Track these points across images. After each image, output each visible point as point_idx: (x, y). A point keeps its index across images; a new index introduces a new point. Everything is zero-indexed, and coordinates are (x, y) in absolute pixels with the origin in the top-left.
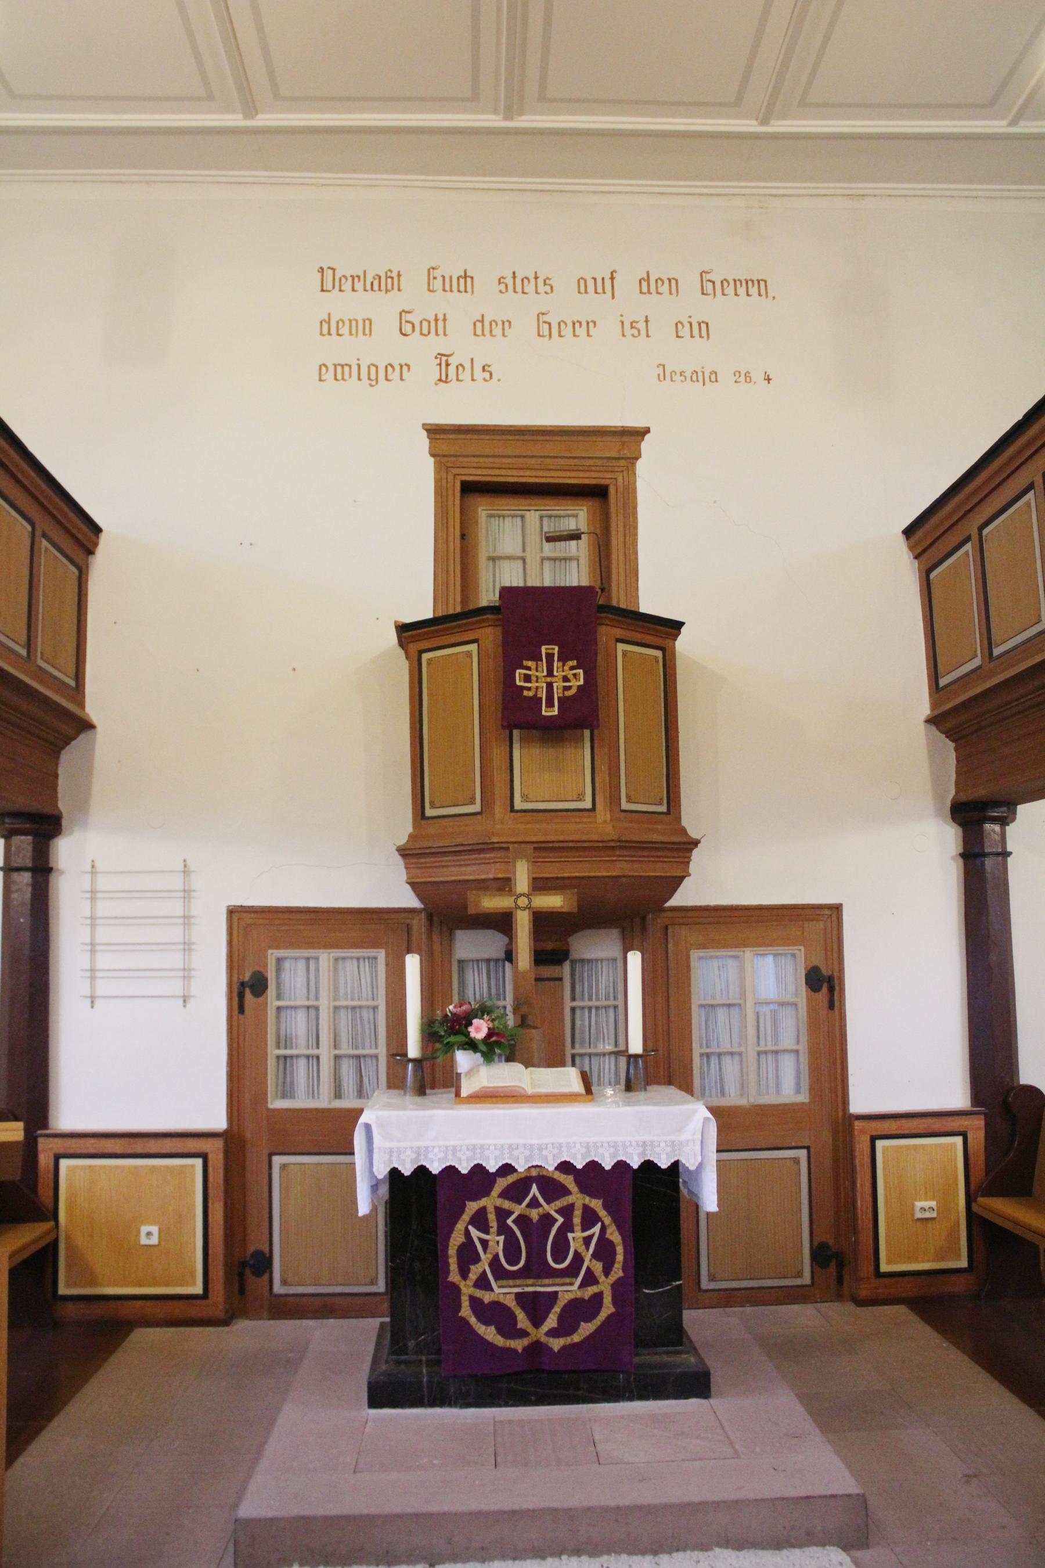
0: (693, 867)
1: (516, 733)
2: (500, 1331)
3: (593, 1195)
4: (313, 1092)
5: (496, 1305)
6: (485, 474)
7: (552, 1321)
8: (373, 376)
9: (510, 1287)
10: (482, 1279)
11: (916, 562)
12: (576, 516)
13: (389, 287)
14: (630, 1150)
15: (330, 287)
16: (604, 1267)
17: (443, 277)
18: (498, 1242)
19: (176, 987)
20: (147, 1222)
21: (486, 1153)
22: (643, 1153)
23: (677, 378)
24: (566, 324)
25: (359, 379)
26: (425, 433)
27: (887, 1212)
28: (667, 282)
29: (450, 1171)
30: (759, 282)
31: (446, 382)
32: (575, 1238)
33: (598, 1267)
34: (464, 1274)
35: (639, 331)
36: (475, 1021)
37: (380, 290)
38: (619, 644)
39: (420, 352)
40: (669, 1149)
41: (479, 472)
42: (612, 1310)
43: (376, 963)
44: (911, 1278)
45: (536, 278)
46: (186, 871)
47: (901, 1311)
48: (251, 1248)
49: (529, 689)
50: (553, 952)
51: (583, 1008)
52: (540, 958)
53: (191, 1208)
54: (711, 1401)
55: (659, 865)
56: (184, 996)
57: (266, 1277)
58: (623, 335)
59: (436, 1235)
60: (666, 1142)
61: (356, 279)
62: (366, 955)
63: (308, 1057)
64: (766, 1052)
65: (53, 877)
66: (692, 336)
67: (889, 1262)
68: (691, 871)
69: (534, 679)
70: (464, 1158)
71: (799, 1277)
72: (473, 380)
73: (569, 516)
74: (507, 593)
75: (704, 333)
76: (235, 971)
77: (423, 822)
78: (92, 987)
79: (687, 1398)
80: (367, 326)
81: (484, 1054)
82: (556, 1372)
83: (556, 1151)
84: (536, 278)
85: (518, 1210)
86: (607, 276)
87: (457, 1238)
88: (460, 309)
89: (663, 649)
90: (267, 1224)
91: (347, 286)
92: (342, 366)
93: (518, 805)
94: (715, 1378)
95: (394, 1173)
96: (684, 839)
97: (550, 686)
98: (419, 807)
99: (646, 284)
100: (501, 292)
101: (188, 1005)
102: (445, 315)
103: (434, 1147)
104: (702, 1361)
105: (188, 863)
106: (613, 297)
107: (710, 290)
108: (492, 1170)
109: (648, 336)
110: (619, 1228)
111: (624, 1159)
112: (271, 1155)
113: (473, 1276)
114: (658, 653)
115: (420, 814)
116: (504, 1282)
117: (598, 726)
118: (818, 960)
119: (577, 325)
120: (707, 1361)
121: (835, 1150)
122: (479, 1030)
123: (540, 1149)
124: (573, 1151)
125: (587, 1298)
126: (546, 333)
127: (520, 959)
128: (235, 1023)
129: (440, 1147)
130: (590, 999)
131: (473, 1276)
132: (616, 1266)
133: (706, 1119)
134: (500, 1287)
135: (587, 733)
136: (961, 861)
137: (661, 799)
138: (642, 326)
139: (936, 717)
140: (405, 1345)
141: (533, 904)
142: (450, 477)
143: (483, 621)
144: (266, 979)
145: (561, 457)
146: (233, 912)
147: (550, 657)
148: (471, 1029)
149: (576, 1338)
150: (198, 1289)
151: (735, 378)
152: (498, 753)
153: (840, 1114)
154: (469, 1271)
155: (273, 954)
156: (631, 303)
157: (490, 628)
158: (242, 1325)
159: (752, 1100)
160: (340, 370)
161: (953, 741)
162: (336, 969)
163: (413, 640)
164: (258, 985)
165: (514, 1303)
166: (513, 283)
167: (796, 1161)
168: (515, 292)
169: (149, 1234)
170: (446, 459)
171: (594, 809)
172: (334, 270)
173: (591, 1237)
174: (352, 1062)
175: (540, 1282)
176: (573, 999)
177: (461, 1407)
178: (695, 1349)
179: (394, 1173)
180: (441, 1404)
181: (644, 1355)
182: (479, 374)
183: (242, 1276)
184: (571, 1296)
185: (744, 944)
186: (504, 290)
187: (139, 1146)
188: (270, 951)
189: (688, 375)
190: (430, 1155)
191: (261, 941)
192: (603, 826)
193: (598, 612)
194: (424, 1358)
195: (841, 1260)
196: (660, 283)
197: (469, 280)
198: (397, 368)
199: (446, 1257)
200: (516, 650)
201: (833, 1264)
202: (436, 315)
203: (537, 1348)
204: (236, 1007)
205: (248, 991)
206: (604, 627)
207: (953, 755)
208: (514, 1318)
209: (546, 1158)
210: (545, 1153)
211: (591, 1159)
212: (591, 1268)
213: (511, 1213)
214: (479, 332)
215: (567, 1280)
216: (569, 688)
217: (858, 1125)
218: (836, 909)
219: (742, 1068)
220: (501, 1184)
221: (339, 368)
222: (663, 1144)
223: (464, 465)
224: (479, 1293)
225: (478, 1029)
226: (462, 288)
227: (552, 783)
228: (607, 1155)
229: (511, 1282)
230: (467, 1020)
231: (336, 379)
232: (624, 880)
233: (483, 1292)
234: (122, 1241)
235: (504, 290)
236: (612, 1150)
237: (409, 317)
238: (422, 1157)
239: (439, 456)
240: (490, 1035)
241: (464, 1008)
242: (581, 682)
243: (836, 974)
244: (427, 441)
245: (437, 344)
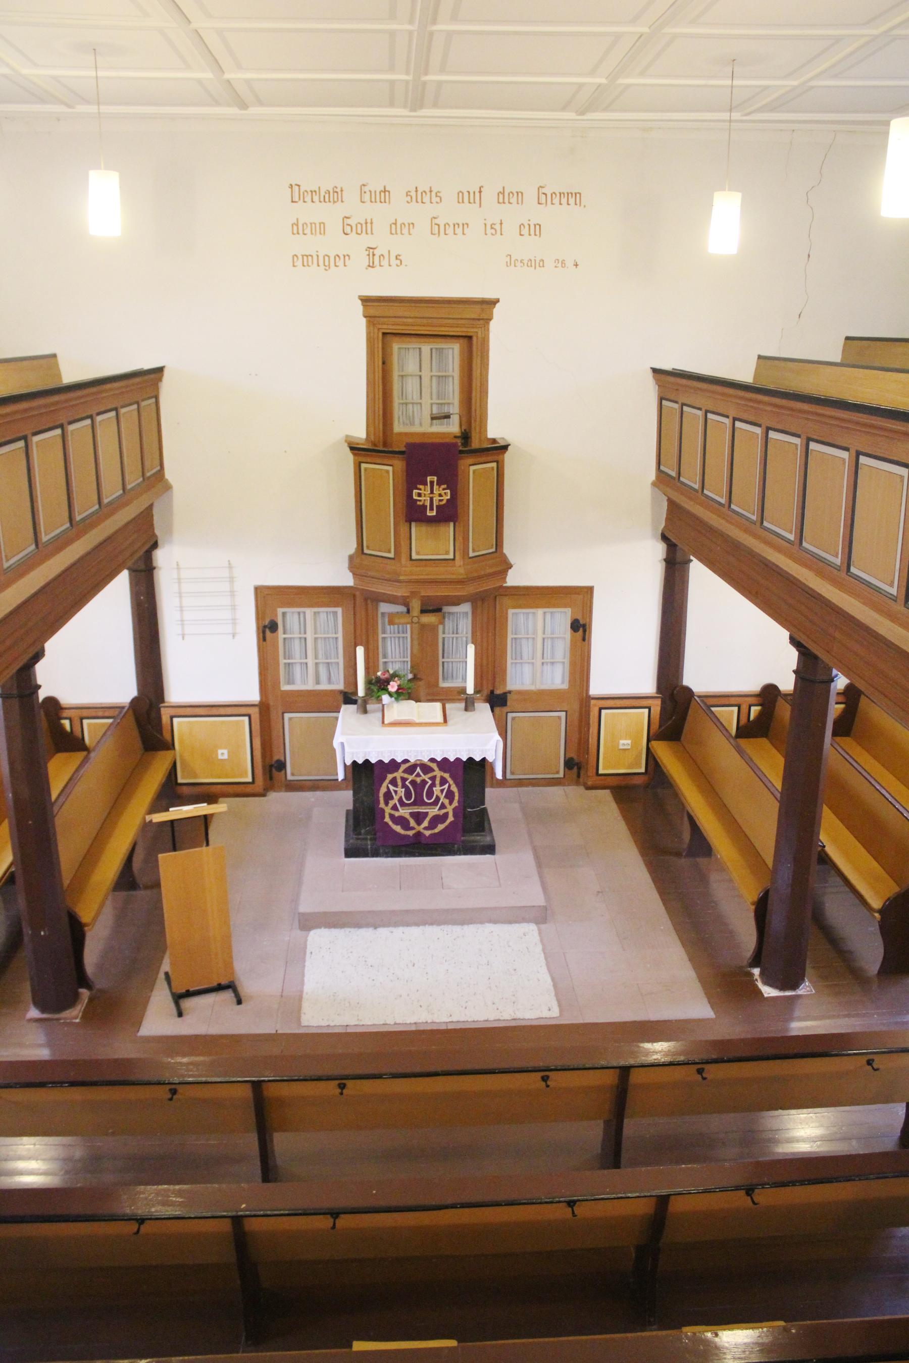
3: (445, 772)
4: (304, 682)
6: (395, 325)
7: (425, 824)
8: (327, 264)
10: (394, 807)
20: (221, 748)
23: (518, 264)
26: (360, 302)
28: (515, 194)
32: (437, 790)
33: (447, 802)
34: (387, 804)
39: (356, 246)
45: (431, 191)
46: (230, 567)
48: (275, 758)
54: (497, 857)
57: (283, 772)
64: (547, 663)
65: (155, 572)
78: (183, 629)
80: (320, 228)
84: (431, 191)
85: (411, 778)
86: (477, 191)
87: (383, 790)
88: (381, 214)
90: (282, 747)
93: (414, 556)
97: (431, 499)
99: (503, 196)
104: (493, 840)
107: (543, 201)
112: (283, 713)
126: (437, 232)
136: (664, 563)
138: (498, 227)
142: (376, 331)
146: (258, 590)
147: (432, 483)
148: (389, 687)
149: (436, 831)
150: (250, 779)
155: (280, 611)
158: (273, 796)
160: (306, 259)
164: (273, 627)
166: (416, 196)
167: (559, 718)
169: (223, 754)
171: (454, 559)
179: (354, 763)
183: (272, 771)
187: (214, 711)
189: (525, 262)
191: (273, 608)
192: (460, 570)
195: (579, 766)
198: (342, 257)
199: (378, 797)
201: (576, 767)
203: (419, 834)
208: (408, 822)
212: (444, 803)
213: (407, 779)
214: (393, 231)
217: (593, 702)
218: (590, 590)
220: (403, 767)
221: (305, 258)
224: (393, 812)
225: (393, 687)
227: (432, 545)
230: (387, 682)
234: (209, 758)
240: (398, 689)
245: (366, 240)
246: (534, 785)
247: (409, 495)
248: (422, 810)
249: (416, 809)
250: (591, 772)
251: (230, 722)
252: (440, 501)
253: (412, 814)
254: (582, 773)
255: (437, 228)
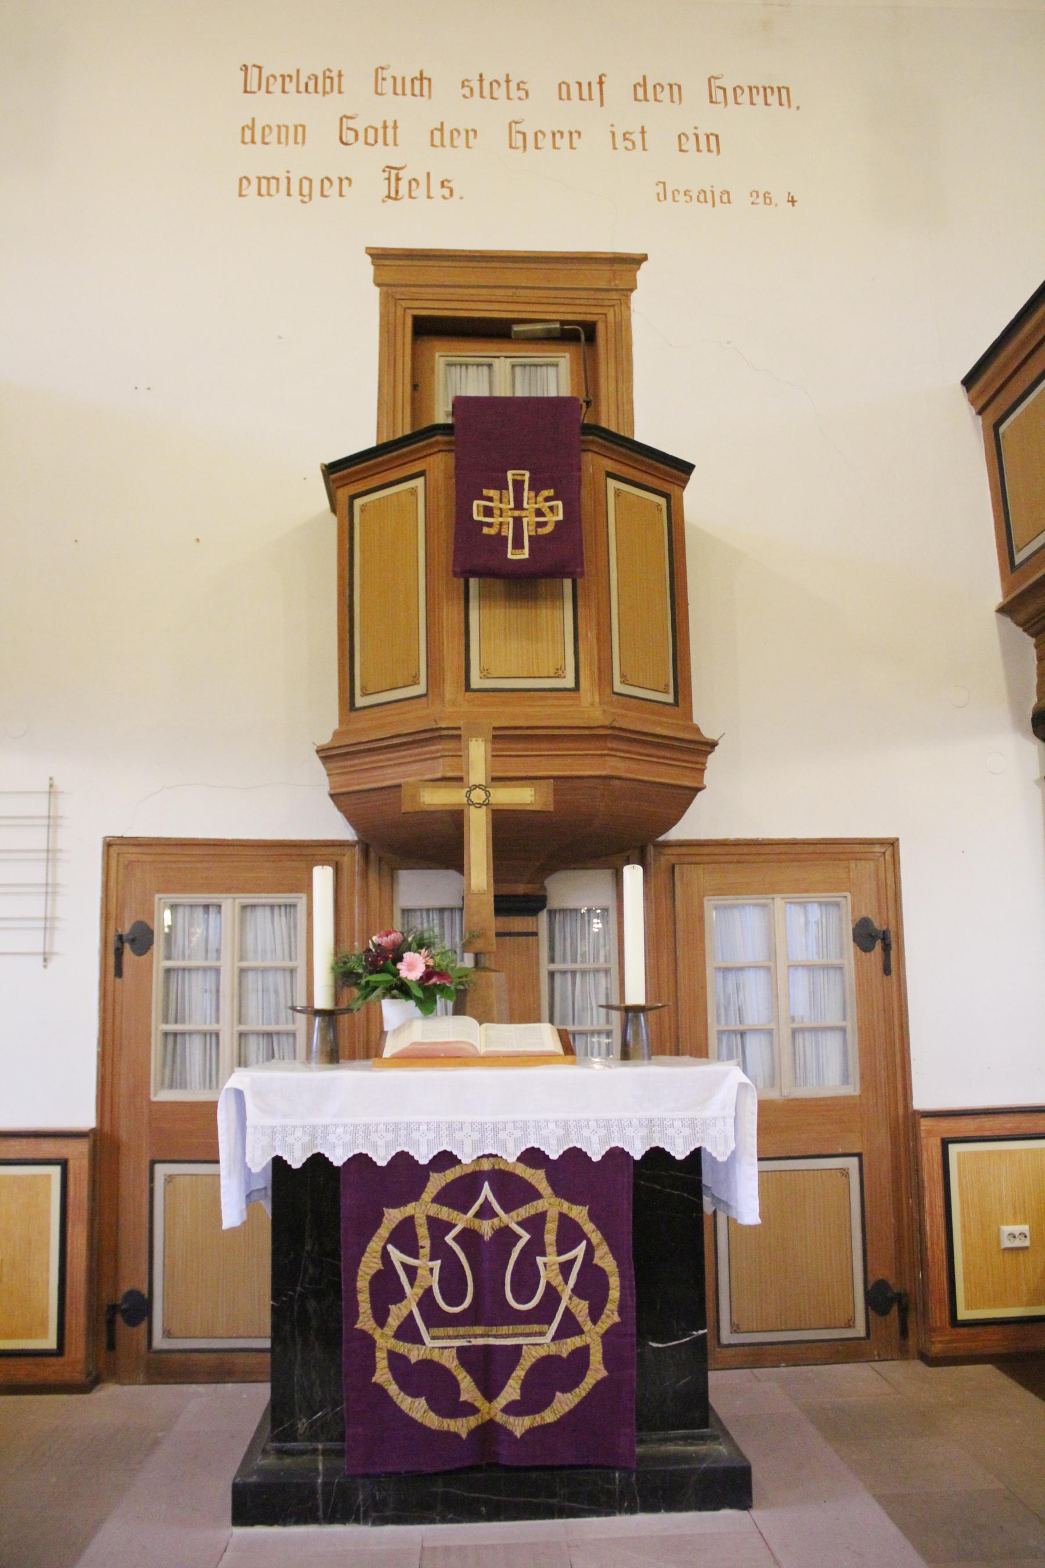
0: (708, 777)
1: (473, 582)
2: (435, 1406)
5: (429, 1366)
6: (436, 311)
7: (512, 1391)
8: (306, 191)
9: (450, 1337)
10: (406, 1325)
11: (980, 418)
12: (556, 365)
13: (328, 89)
14: (629, 1132)
15: (255, 88)
16: (590, 1308)
17: (395, 79)
18: (431, 1270)
19: (35, 942)
21: (415, 1135)
22: (649, 1136)
23: (681, 197)
24: (544, 134)
25: (289, 195)
26: (369, 259)
27: (964, 1242)
28: (667, 88)
29: (361, 1161)
30: (779, 89)
31: (396, 199)
32: (548, 1265)
33: (581, 1308)
34: (381, 1318)
35: (633, 143)
36: (408, 956)
37: (316, 91)
38: (610, 481)
39: (366, 165)
40: (687, 1131)
41: (436, 305)
42: (603, 1373)
43: (296, 912)
44: (998, 1329)
45: (508, 81)
46: (52, 791)
47: (987, 1372)
48: (125, 1288)
49: (490, 525)
50: (526, 898)
51: (564, 973)
52: (506, 905)
53: (45, 1231)
55: (663, 769)
56: (45, 953)
57: (144, 1325)
58: (615, 148)
59: (340, 1260)
60: (682, 1120)
61: (287, 79)
62: (281, 901)
63: (205, 1034)
66: (698, 150)
67: (969, 1307)
68: (705, 782)
69: (497, 512)
70: (381, 1143)
71: (850, 1327)
72: (429, 197)
73: (547, 365)
74: (461, 404)
75: (713, 146)
76: (112, 922)
77: (354, 714)
79: (717, 1508)
80: (300, 133)
81: (420, 1003)
82: (518, 1469)
83: (518, 1133)
84: (508, 81)
85: (462, 1221)
87: (369, 1265)
88: (414, 116)
89: (666, 496)
91: (276, 87)
92: (268, 179)
93: (476, 682)
94: (757, 1476)
95: (278, 1164)
96: (697, 738)
97: (518, 522)
98: (348, 695)
100: (464, 96)
101: (50, 965)
102: (395, 122)
103: (336, 1126)
105: (56, 782)
106: (602, 104)
108: (424, 1161)
109: (644, 149)
110: (614, 1249)
111: (621, 1145)
112: (153, 1163)
113: (394, 1321)
114: (662, 501)
115: (348, 704)
116: (440, 1331)
117: (582, 574)
118: (868, 911)
119: (558, 136)
120: (744, 1449)
121: (895, 1156)
122: (412, 967)
123: (495, 1129)
124: (545, 1132)
125: (565, 1355)
126: (520, 143)
127: (473, 873)
128: (110, 988)
129: (345, 1126)
130: (574, 960)
131: (394, 1321)
132: (608, 1306)
133: (742, 1086)
134: (433, 1338)
135: (568, 583)
137: (667, 685)
138: (637, 138)
139: (1010, 603)
140: (293, 1426)
141: (492, 800)
142: (400, 312)
143: (431, 445)
144: (152, 932)
145: (539, 288)
147: (518, 485)
149: (549, 1416)
150: (50, 1342)
151: (752, 199)
152: (451, 614)
153: (901, 1112)
154: (387, 1313)
156: (623, 111)
157: (440, 455)
158: (109, 1392)
159: (785, 1093)
160: (266, 184)
161: (1032, 635)
162: (242, 922)
163: (344, 483)
165: (456, 1362)
166: (481, 87)
168: (482, 96)
170: (394, 289)
172: (260, 68)
173: (571, 1262)
174: (263, 1042)
175: (494, 1330)
176: (552, 960)
177: (374, 1523)
178: (727, 1433)
179: (278, 1164)
180: (344, 1520)
181: (652, 1441)
182: (436, 190)
184: (542, 1352)
185: (773, 889)
186: (468, 95)
188: (157, 896)
190: (332, 1138)
192: (590, 708)
193: (583, 434)
194: (320, 1446)
196: (659, 88)
197: (426, 82)
198: (336, 182)
199: (354, 1291)
200: (473, 478)
201: (895, 1310)
202: (385, 122)
203: (490, 1430)
204: (111, 970)
205: (127, 947)
206: (590, 455)
207: (1034, 652)
209: (504, 1145)
210: (502, 1135)
211: (571, 1145)
212: (573, 1315)
213: (451, 1226)
214: (437, 142)
215: (536, 1328)
216: (543, 524)
217: (925, 1124)
218: (893, 844)
219: (772, 1051)
220: (437, 1182)
221: (264, 182)
222: (677, 1124)
223: (417, 296)
224: (402, 1348)
225: (411, 967)
226: (417, 91)
227: (522, 653)
228: (595, 1139)
229: (451, 1331)
231: (260, 194)
232: (617, 782)
233: (409, 1346)
235: (468, 95)
236: (602, 1132)
237: (351, 123)
238: (319, 1141)
239: (387, 285)
240: (429, 974)
241: (392, 937)
242: (560, 517)
243: (892, 929)
244: (372, 268)
246: (795, 1362)
247: (463, 511)
248: (501, 1338)
249: (481, 1338)
250: (939, 1315)
251: (16, 1178)
252: (540, 525)
253: (463, 1353)
254: (912, 1318)
255: (518, 138)
